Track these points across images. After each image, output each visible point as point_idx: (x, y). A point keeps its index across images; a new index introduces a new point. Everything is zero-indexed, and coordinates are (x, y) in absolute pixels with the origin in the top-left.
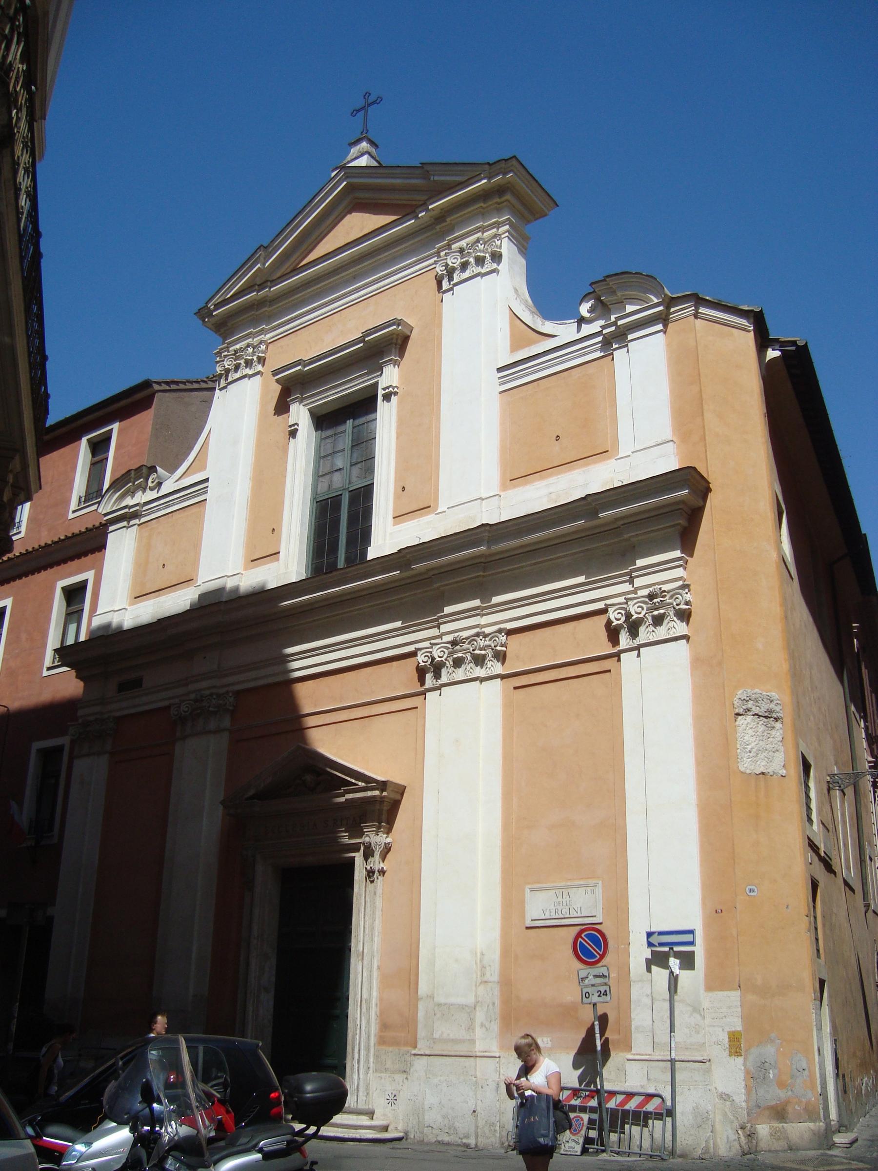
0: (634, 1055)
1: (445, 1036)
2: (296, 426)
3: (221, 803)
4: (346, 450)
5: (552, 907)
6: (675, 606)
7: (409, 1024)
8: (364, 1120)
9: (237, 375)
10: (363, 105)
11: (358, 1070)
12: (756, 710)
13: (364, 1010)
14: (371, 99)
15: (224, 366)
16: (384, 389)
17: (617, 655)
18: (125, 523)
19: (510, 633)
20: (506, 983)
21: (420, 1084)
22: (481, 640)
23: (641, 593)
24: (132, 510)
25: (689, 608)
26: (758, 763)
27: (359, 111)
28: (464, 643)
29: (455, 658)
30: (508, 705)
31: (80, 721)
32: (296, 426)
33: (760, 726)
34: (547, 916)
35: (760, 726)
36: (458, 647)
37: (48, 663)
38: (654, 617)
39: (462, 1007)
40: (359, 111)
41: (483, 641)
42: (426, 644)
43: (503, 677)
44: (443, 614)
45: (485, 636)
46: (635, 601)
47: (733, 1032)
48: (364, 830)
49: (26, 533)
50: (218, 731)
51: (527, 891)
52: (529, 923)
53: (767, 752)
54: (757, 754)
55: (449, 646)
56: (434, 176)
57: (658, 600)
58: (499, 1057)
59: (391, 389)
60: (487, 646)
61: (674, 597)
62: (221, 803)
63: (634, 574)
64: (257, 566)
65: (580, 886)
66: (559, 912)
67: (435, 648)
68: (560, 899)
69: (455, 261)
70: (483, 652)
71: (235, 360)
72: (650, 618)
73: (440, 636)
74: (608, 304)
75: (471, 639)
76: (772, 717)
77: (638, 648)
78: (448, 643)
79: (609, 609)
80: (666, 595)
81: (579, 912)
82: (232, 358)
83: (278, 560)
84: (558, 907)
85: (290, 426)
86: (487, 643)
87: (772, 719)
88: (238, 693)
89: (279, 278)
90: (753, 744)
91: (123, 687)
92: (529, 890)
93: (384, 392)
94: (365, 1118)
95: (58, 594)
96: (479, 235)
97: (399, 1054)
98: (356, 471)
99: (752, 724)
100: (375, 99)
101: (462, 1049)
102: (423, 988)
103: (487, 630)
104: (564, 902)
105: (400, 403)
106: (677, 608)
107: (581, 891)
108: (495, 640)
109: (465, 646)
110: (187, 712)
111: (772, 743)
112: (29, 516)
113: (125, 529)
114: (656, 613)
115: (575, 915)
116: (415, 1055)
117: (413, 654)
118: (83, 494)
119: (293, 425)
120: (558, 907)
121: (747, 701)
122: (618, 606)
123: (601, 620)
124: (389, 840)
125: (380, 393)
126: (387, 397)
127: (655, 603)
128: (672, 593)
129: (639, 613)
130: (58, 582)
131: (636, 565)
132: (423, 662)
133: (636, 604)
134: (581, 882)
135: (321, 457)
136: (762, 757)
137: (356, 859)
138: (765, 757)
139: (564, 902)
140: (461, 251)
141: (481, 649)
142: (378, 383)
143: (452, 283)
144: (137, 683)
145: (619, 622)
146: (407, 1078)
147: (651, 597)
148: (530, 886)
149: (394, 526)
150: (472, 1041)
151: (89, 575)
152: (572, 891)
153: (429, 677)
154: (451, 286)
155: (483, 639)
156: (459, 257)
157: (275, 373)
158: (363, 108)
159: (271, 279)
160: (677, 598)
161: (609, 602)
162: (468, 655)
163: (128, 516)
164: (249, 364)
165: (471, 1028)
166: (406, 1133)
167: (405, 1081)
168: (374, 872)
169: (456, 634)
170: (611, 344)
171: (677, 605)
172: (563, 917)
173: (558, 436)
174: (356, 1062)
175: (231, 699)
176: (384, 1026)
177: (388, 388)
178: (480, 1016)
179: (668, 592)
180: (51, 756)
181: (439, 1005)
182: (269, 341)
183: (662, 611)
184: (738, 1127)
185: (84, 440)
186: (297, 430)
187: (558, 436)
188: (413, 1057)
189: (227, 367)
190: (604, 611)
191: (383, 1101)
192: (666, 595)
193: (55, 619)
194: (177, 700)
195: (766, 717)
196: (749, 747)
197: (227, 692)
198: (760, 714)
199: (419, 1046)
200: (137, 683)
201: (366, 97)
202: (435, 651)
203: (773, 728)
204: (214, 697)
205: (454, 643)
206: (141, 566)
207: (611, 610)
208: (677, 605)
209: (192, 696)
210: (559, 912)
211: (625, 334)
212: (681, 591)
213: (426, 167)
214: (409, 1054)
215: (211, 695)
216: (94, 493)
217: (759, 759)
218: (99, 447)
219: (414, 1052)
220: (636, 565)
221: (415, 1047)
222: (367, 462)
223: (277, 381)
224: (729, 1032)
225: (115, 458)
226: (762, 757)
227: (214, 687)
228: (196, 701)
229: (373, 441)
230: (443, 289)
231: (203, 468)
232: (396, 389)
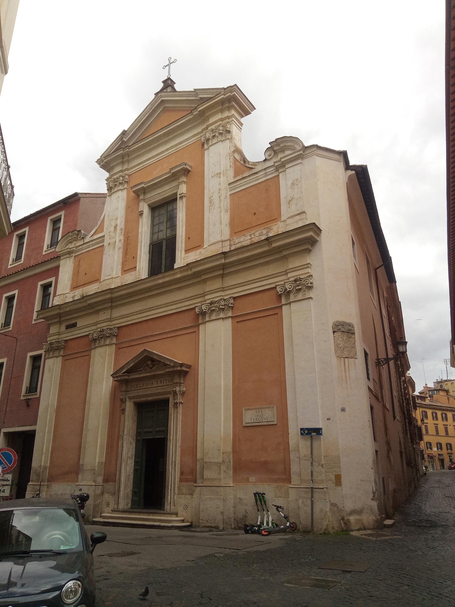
0: (292, 485)
1: (208, 477)
2: (142, 212)
3: (112, 375)
4: (164, 222)
6: (306, 285)
7: (193, 472)
8: (174, 518)
9: (116, 190)
10: (168, 64)
11: (171, 494)
12: (343, 330)
13: (173, 466)
14: (171, 61)
15: (110, 186)
16: (180, 195)
17: (281, 307)
18: (68, 256)
19: (234, 298)
20: (234, 451)
22: (222, 302)
23: (291, 280)
24: (71, 250)
25: (312, 286)
26: (344, 353)
27: (166, 66)
28: (215, 303)
29: (211, 310)
30: (234, 329)
31: (49, 343)
32: (142, 212)
33: (345, 337)
35: (345, 337)
36: (213, 305)
37: (35, 318)
38: (296, 290)
39: (216, 463)
40: (166, 66)
41: (233, 300)
42: (199, 304)
43: (232, 317)
45: (224, 300)
46: (288, 283)
47: (337, 475)
49: (24, 262)
50: (110, 345)
51: (244, 410)
52: (244, 425)
53: (348, 348)
54: (344, 349)
56: (200, 95)
57: (299, 282)
58: (233, 487)
59: (183, 195)
60: (225, 304)
62: (112, 375)
63: (288, 271)
64: (127, 273)
65: (266, 408)
66: (258, 420)
69: (210, 135)
70: (223, 307)
71: (114, 183)
72: (295, 290)
73: (205, 301)
74: (277, 151)
75: (218, 302)
76: (350, 333)
77: (290, 303)
78: (208, 303)
79: (277, 287)
80: (302, 280)
81: (266, 420)
82: (113, 182)
83: (136, 270)
84: (257, 417)
85: (140, 212)
86: (226, 303)
87: (350, 334)
88: (119, 328)
89: (132, 145)
90: (342, 345)
91: (68, 327)
92: (244, 410)
93: (180, 196)
94: (174, 516)
95: (39, 287)
96: (221, 122)
97: (189, 486)
98: (169, 231)
99: (341, 336)
100: (174, 60)
101: (216, 484)
102: (199, 455)
103: (225, 298)
104: (260, 415)
105: (187, 201)
106: (307, 285)
107: (267, 410)
108: (228, 302)
109: (216, 305)
110: (282, 291)
111: (350, 344)
113: (68, 258)
114: (297, 288)
115: (265, 421)
116: (196, 486)
117: (194, 308)
118: (49, 244)
119: (141, 211)
120: (257, 417)
121: (339, 326)
122: (281, 286)
123: (273, 292)
124: (184, 389)
125: (178, 196)
126: (181, 198)
127: (297, 284)
128: (304, 279)
129: (290, 288)
130: (39, 283)
132: (198, 312)
133: (288, 284)
134: (267, 406)
135: (153, 226)
136: (346, 350)
137: (170, 398)
138: (348, 350)
139: (260, 415)
140: (212, 130)
141: (222, 306)
142: (177, 192)
143: (208, 145)
144: (74, 325)
145: (281, 293)
146: (192, 497)
147: (296, 281)
148: (244, 408)
149: (185, 254)
150: (220, 479)
151: (53, 279)
152: (263, 410)
153: (200, 318)
154: (208, 147)
155: (224, 301)
156: (211, 134)
157: (132, 188)
158: (168, 65)
159: (129, 146)
160: (307, 281)
161: (277, 284)
162: (217, 308)
163: (70, 253)
164: (121, 184)
165: (220, 473)
166: (192, 523)
167: (191, 498)
168: (177, 403)
169: (212, 300)
170: (278, 170)
171: (307, 284)
173: (255, 213)
174: (170, 490)
175: (116, 331)
176: (182, 473)
177: (182, 194)
178: (223, 468)
179: (303, 279)
180: (36, 359)
181: (206, 463)
182: (129, 174)
183: (300, 287)
184: (341, 519)
185: (49, 219)
186: (143, 213)
187: (255, 213)
188: (194, 487)
189: (111, 186)
190: (275, 288)
191: (181, 508)
192: (302, 280)
193: (38, 299)
194: (92, 332)
195: (347, 332)
196: (340, 346)
197: (114, 328)
198: (344, 331)
199: (197, 482)
200: (74, 325)
201: (169, 59)
202: (203, 307)
203: (351, 337)
204: (109, 330)
205: (211, 303)
206: (76, 273)
207: (278, 287)
208: (307, 284)
209: (99, 330)
210: (258, 420)
211: (285, 165)
212: (308, 278)
213: (196, 91)
214: (193, 486)
215: (107, 329)
216: (54, 243)
217: (345, 351)
218: (56, 222)
219: (195, 485)
221: (196, 482)
222: (173, 226)
223: (134, 192)
224: (335, 475)
225: (63, 228)
226: (346, 350)
227: (109, 325)
228: (100, 331)
229: (175, 218)
230: (205, 148)
231: (102, 231)
232: (185, 195)
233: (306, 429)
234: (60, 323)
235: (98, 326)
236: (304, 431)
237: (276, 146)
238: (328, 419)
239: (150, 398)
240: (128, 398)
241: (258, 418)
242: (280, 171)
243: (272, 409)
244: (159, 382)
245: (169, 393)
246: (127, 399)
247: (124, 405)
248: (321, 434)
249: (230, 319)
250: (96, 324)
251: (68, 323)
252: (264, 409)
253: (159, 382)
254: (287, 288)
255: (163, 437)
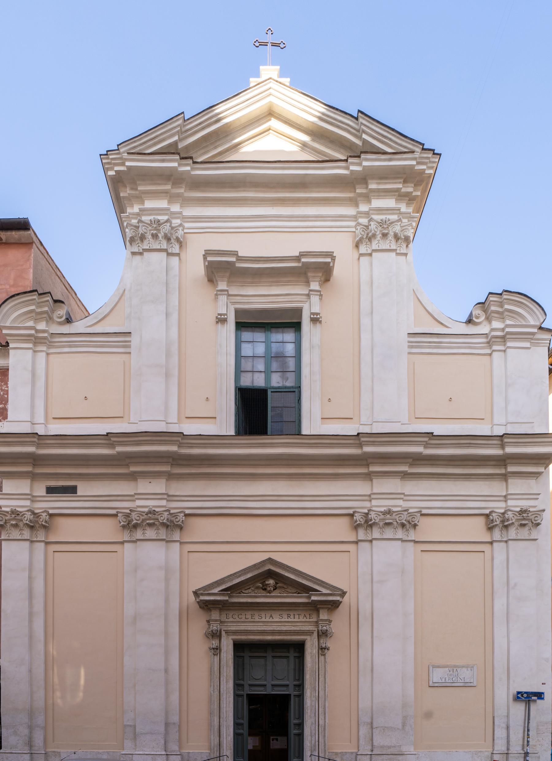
5: (446, 676)
21: (450, 754)
34: (443, 681)
44: (76, 495)
46: (136, 513)
48: (320, 622)
55: (517, 514)
61: (175, 517)
66: (451, 680)
67: (133, 514)
68: (451, 672)
75: (399, 513)
89: (202, 163)
112: (222, 150)
115: (461, 681)
131: (77, 494)
133: (136, 514)
144: (72, 490)
145: (125, 524)
152: (459, 670)
170: (490, 347)
172: (453, 682)
179: (157, 512)
220: (77, 494)
233: (525, 693)
234: (33, 477)
235: (139, 503)
236: (522, 695)
237: (494, 305)
238: (543, 684)
239: (269, 638)
240: (224, 633)
241: (451, 677)
242: (495, 347)
243: (470, 668)
244: (292, 617)
245: (310, 633)
246: (223, 633)
247: (218, 641)
248: (543, 699)
249: (178, 544)
250: (132, 498)
251: (53, 483)
252: (460, 669)
253: (292, 617)
254: (134, 519)
255: (287, 693)
